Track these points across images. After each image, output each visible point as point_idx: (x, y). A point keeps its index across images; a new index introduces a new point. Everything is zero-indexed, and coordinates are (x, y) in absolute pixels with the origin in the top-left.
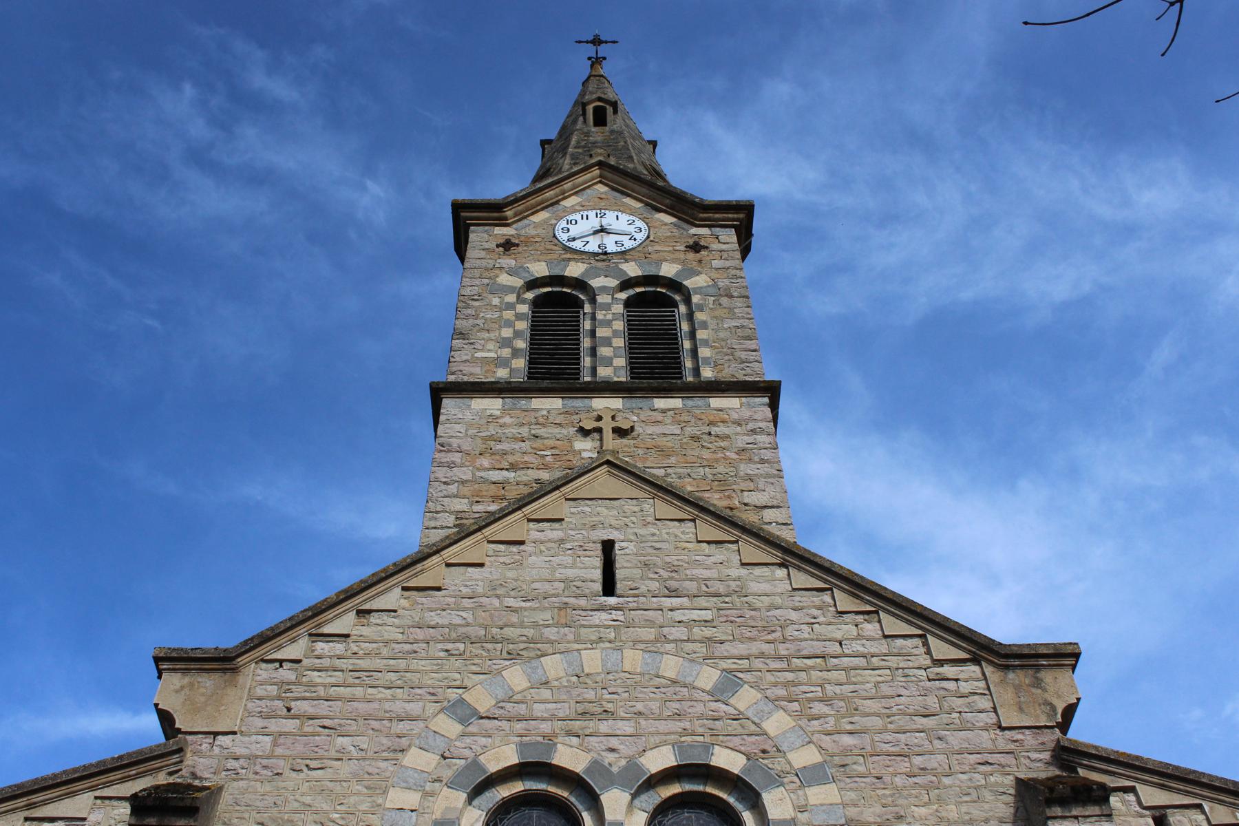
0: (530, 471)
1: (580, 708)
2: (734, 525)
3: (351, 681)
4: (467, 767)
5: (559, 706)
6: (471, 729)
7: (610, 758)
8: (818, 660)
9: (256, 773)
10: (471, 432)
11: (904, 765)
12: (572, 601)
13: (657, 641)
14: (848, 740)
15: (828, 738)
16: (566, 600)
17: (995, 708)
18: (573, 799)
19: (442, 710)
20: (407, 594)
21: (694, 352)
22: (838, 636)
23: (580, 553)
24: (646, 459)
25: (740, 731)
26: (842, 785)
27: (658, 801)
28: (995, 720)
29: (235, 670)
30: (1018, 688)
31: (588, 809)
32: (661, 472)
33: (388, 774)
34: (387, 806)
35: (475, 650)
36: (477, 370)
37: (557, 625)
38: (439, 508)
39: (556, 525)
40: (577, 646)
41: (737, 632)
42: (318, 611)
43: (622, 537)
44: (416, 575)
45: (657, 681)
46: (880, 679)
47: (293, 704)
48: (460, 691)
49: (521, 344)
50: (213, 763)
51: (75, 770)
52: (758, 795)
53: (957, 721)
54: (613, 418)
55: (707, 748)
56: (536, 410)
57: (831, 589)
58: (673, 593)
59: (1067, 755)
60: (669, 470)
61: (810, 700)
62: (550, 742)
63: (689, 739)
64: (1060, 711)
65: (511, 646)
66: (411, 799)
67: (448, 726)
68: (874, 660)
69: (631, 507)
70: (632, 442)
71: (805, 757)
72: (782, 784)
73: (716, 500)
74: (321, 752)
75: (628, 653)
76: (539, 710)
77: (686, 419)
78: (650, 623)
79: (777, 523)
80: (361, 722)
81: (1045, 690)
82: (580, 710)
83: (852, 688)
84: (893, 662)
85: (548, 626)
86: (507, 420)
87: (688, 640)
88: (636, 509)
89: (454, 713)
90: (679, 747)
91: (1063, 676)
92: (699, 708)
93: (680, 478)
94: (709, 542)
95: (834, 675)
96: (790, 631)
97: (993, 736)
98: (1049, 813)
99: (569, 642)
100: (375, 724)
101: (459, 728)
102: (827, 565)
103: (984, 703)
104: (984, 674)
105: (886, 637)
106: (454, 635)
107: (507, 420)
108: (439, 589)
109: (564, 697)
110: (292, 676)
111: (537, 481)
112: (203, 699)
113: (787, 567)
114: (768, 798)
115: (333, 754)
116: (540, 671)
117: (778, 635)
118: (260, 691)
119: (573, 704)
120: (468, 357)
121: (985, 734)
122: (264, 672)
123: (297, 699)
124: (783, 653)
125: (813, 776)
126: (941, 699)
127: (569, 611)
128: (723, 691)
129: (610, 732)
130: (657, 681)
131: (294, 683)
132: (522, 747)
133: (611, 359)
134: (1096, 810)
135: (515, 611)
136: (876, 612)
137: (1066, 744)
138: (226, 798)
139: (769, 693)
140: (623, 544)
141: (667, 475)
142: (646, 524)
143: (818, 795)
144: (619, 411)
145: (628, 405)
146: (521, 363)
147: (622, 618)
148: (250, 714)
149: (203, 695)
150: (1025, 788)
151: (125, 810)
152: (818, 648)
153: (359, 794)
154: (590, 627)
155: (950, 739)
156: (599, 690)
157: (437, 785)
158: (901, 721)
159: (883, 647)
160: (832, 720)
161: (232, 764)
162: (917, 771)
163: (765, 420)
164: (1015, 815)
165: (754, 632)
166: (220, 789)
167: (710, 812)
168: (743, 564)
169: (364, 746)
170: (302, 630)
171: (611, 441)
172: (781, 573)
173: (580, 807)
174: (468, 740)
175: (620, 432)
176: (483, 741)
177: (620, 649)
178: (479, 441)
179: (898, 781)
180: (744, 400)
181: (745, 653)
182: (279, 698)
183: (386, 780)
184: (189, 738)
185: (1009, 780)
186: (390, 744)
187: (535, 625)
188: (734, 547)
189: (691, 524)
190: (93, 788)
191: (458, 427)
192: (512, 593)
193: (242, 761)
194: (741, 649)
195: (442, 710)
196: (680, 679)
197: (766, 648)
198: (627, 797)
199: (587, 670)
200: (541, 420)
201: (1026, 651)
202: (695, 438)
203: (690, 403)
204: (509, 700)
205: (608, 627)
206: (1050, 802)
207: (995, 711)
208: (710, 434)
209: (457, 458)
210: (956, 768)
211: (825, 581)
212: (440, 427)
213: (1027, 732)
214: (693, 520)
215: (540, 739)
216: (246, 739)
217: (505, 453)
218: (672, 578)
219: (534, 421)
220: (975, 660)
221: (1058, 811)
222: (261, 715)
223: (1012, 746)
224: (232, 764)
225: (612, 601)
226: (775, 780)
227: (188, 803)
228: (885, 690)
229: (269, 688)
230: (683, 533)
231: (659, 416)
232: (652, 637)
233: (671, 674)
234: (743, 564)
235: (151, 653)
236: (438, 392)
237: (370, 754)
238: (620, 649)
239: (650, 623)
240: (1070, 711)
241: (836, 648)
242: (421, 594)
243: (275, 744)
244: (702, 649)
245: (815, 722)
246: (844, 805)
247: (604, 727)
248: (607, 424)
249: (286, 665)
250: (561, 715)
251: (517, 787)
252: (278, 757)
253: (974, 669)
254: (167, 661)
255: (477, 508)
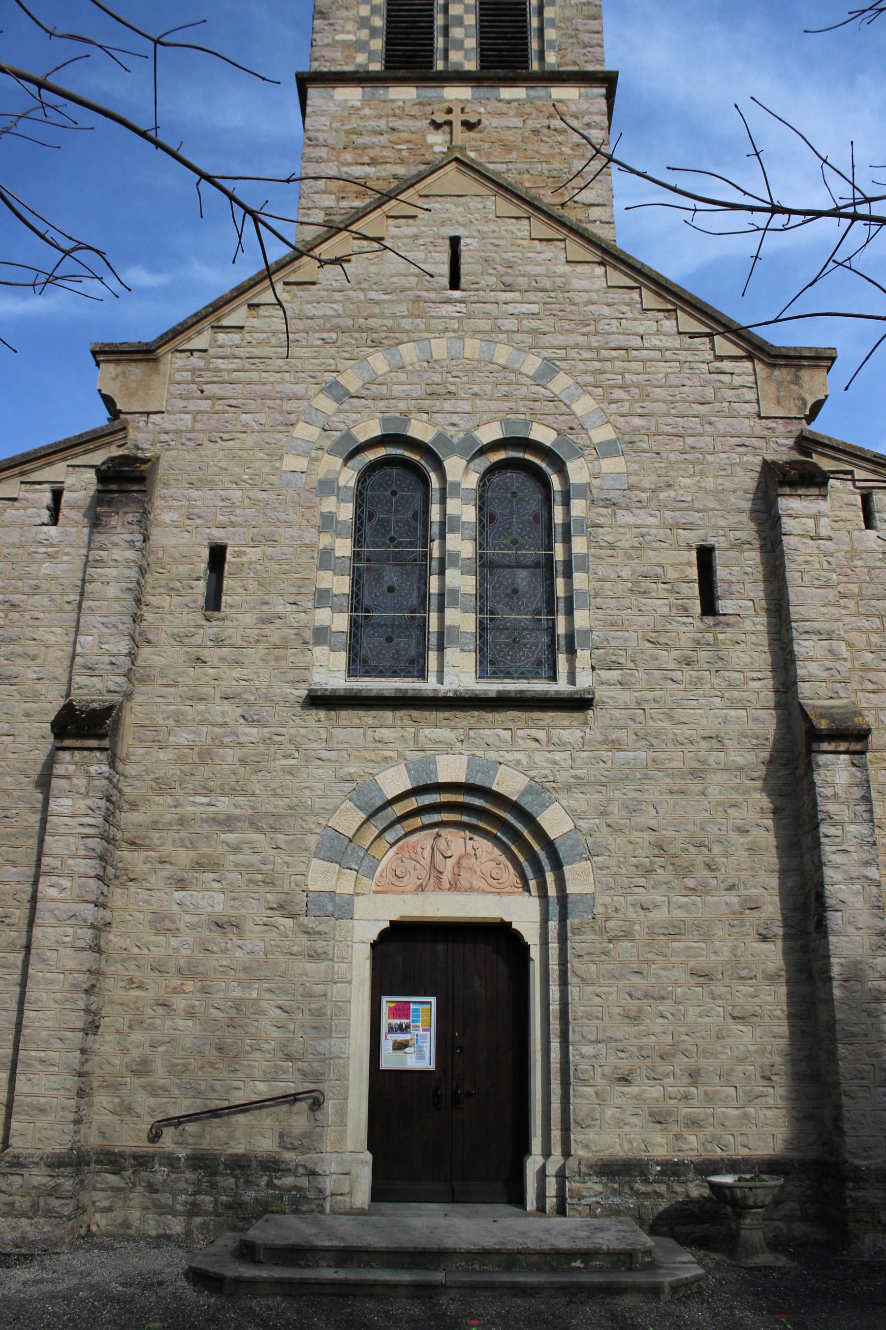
0: (388, 166)
1: (429, 389)
2: (563, 224)
3: (248, 366)
4: (343, 438)
5: (413, 387)
6: (345, 406)
7: (452, 431)
8: (622, 352)
9: (183, 444)
10: (336, 125)
11: (678, 444)
12: (424, 294)
13: (492, 331)
14: (637, 422)
15: (622, 419)
16: (418, 293)
17: (758, 400)
18: (423, 462)
19: (321, 391)
20: (288, 288)
21: (541, 31)
22: (641, 331)
23: (431, 248)
24: (491, 154)
25: (554, 411)
26: (629, 458)
27: (488, 464)
28: (756, 410)
29: (156, 360)
30: (779, 384)
31: (434, 470)
32: (502, 168)
33: (282, 444)
34: (284, 469)
35: (346, 338)
36: (338, 55)
37: (412, 316)
38: (310, 205)
39: (411, 221)
40: (427, 335)
41: (558, 324)
42: (217, 306)
43: (467, 234)
44: (294, 271)
45: (491, 367)
46: (670, 370)
47: (205, 387)
48: (335, 374)
49: (379, 22)
50: (150, 436)
51: (49, 446)
52: (563, 464)
53: (726, 410)
54: (463, 110)
55: (527, 424)
56: (393, 101)
57: (640, 288)
58: (508, 288)
59: (806, 444)
60: (511, 166)
61: (612, 387)
62: (429, 764)
63: (513, 416)
64: (809, 406)
65: (374, 335)
66: (301, 463)
67: (326, 404)
68: (668, 353)
69: (475, 203)
70: (479, 135)
71: (602, 434)
72: (583, 456)
73: (548, 199)
74: (230, 427)
75: (469, 342)
76: (397, 390)
77: (528, 110)
78: (487, 315)
79: (601, 222)
80: (259, 401)
81: (801, 387)
82: (429, 392)
83: (646, 377)
84: (683, 355)
85: (404, 317)
86: (367, 111)
87: (518, 331)
88: (480, 206)
89: (331, 393)
90: (505, 423)
91: (819, 375)
92: (523, 391)
93: (519, 173)
94: (540, 240)
95: (633, 365)
96: (602, 326)
97: (752, 423)
98: (780, 491)
99: (421, 331)
100: (270, 403)
101: (335, 405)
102: (638, 266)
103: (750, 395)
104: (754, 370)
105: (680, 333)
106: (328, 326)
107: (367, 111)
108: (314, 283)
109: (417, 380)
110: (201, 364)
111: (395, 177)
112: (134, 385)
113: (605, 266)
114: (571, 466)
115: (240, 428)
116: (398, 357)
117: (591, 328)
118: (178, 377)
119: (424, 385)
120: (329, 41)
121: (746, 421)
122: (179, 360)
123: (207, 383)
124: (595, 344)
125: (608, 449)
126: (716, 390)
127: (421, 303)
128: (542, 377)
129: (453, 410)
130: (491, 367)
131: (203, 370)
132: (384, 422)
133: (462, 42)
134: (816, 491)
135: (377, 303)
136: (675, 311)
137: (808, 435)
138: (163, 465)
139: (579, 379)
140: (469, 241)
141: (508, 171)
142: (488, 221)
143: (612, 465)
144: (468, 101)
145: (476, 95)
146: (378, 44)
147: (464, 310)
148: (173, 396)
149: (134, 381)
150: (768, 468)
151: (91, 475)
152: (622, 340)
153: (261, 459)
154: (439, 318)
155: (718, 424)
156: (444, 374)
157: (320, 452)
158: (682, 407)
159: (676, 342)
160: (627, 404)
161: (164, 437)
162: (688, 449)
163: (600, 113)
164: (757, 488)
165: (572, 325)
166: (158, 458)
167: (527, 472)
168: (568, 262)
169: (263, 422)
170: (206, 323)
171: (461, 136)
172: (599, 270)
173: (428, 468)
174: (342, 416)
175: (469, 126)
176: (354, 416)
177: (462, 338)
178: (343, 134)
179: (673, 456)
180: (582, 90)
181: (563, 344)
182: (193, 382)
183: (281, 448)
184: (129, 417)
185: (758, 460)
186: (282, 419)
187: (394, 316)
188: (561, 245)
189: (526, 222)
190: (64, 459)
191: (323, 120)
192: (374, 287)
193: (171, 435)
194: (560, 340)
195: (321, 391)
196: (510, 365)
197: (581, 340)
198: (464, 462)
199: (435, 357)
200: (398, 111)
201: (792, 353)
202: (536, 132)
203: (533, 93)
204: (373, 382)
205: (453, 318)
206: (782, 484)
207: (758, 403)
208: (549, 127)
209: (323, 152)
210: (719, 447)
211: (636, 280)
212: (307, 119)
213: (780, 421)
214: (529, 218)
215: (398, 415)
216: (172, 417)
217: (365, 147)
218: (507, 274)
219: (391, 112)
220: (750, 358)
221: (787, 490)
222: (181, 397)
223: (766, 433)
224: (164, 437)
225: (457, 294)
226: (577, 452)
227: (138, 474)
228: (673, 380)
229: (185, 374)
230: (519, 230)
231: (503, 107)
232: (488, 328)
233: (502, 361)
234: (568, 262)
235: (89, 348)
236: (304, 82)
237: (267, 428)
238: (462, 338)
239: (487, 315)
240: (817, 406)
241: (638, 342)
242: (300, 287)
243: (195, 420)
244: (528, 339)
245: (614, 406)
246: (629, 474)
247: (447, 406)
248: (457, 118)
249: (196, 354)
250: (414, 395)
251: (381, 452)
252: (198, 431)
253: (748, 365)
254: (104, 354)
255: (344, 204)
